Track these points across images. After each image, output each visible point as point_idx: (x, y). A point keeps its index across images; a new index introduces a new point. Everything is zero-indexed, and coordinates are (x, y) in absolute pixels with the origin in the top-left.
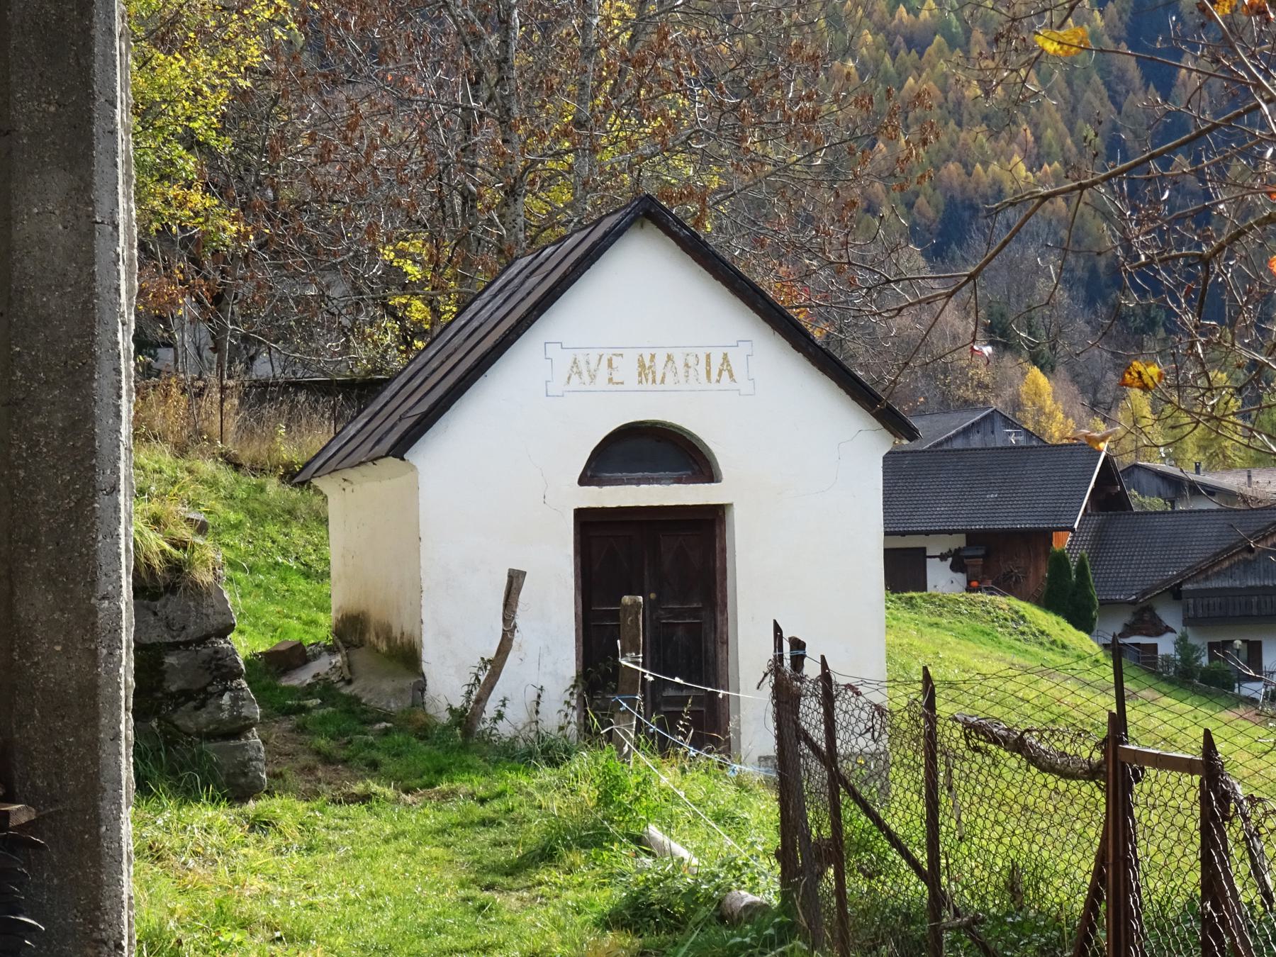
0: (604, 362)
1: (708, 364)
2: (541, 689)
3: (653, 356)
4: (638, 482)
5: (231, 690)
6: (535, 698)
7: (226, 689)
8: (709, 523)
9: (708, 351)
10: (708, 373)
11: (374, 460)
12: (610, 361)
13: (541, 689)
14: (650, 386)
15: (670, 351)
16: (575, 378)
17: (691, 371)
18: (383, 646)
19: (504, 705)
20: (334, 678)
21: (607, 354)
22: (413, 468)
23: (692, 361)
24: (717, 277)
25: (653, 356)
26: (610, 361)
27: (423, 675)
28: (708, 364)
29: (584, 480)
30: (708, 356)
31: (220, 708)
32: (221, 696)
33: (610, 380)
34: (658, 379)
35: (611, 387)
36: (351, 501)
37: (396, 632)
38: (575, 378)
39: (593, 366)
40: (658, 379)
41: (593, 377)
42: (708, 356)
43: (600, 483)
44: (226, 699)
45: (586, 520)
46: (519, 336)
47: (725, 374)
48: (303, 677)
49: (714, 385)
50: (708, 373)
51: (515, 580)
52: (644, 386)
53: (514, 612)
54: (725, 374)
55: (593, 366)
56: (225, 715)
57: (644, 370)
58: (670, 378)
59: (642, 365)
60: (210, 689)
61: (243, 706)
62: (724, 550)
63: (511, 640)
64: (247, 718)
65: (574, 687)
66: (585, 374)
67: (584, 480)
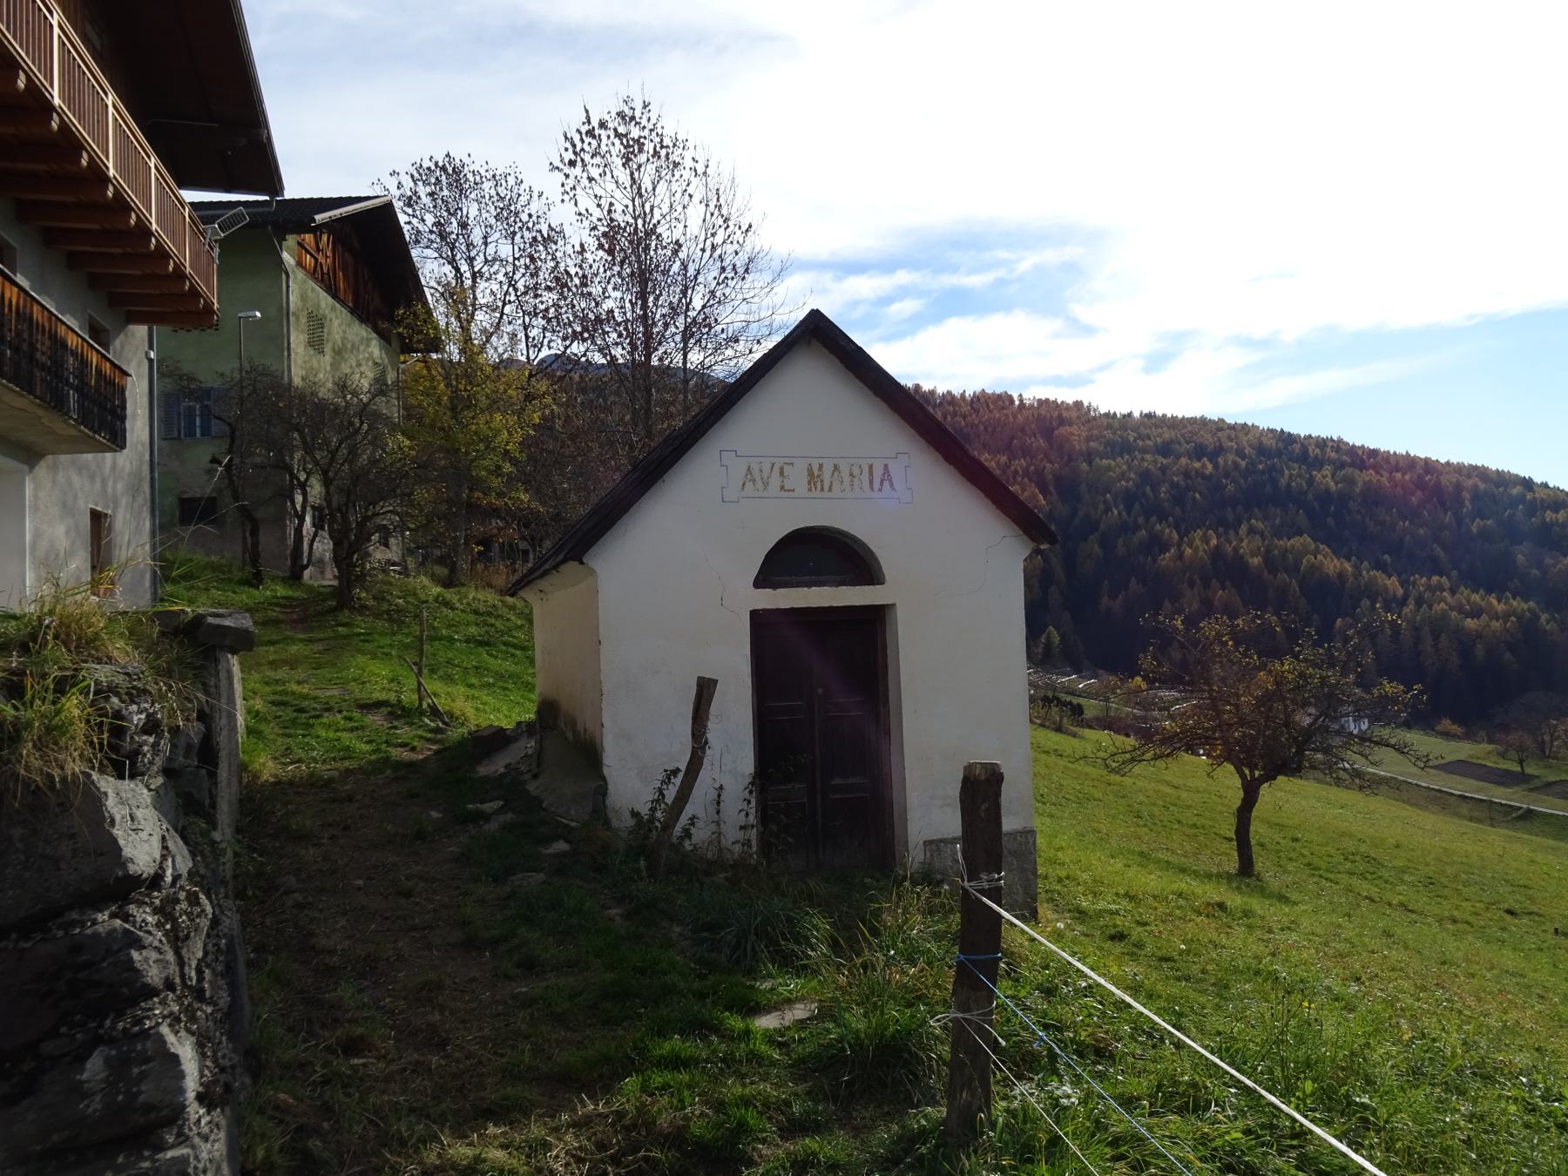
0: (776, 470)
1: (871, 474)
2: (721, 787)
3: (821, 466)
4: (809, 585)
5: (111, 1042)
6: (714, 794)
7: (96, 1041)
8: (875, 620)
9: (871, 461)
10: (871, 482)
11: (556, 567)
12: (782, 470)
13: (721, 787)
14: (818, 494)
15: (837, 461)
16: (749, 485)
17: (856, 481)
18: (570, 736)
19: (693, 824)
20: (523, 768)
21: (779, 462)
22: (593, 572)
23: (856, 471)
24: (876, 394)
25: (821, 466)
26: (782, 470)
27: (604, 778)
28: (871, 474)
29: (761, 582)
30: (871, 467)
31: (79, 1091)
32: (81, 1059)
33: (782, 488)
34: (826, 487)
35: (783, 494)
36: (550, 607)
37: (580, 727)
38: (749, 485)
39: (765, 474)
40: (826, 487)
41: (766, 485)
42: (871, 467)
43: (774, 586)
44: (94, 1068)
45: (761, 621)
46: (697, 440)
47: (886, 483)
48: (495, 766)
49: (876, 494)
50: (871, 482)
51: (705, 689)
52: (814, 494)
53: (705, 726)
54: (886, 483)
55: (765, 474)
56: (96, 1105)
57: (813, 478)
58: (836, 487)
59: (811, 473)
60: (48, 1047)
61: (143, 1076)
62: (885, 647)
63: (702, 758)
64: (149, 1108)
65: (752, 783)
66: (759, 483)
67: (761, 582)
